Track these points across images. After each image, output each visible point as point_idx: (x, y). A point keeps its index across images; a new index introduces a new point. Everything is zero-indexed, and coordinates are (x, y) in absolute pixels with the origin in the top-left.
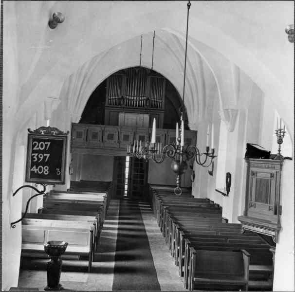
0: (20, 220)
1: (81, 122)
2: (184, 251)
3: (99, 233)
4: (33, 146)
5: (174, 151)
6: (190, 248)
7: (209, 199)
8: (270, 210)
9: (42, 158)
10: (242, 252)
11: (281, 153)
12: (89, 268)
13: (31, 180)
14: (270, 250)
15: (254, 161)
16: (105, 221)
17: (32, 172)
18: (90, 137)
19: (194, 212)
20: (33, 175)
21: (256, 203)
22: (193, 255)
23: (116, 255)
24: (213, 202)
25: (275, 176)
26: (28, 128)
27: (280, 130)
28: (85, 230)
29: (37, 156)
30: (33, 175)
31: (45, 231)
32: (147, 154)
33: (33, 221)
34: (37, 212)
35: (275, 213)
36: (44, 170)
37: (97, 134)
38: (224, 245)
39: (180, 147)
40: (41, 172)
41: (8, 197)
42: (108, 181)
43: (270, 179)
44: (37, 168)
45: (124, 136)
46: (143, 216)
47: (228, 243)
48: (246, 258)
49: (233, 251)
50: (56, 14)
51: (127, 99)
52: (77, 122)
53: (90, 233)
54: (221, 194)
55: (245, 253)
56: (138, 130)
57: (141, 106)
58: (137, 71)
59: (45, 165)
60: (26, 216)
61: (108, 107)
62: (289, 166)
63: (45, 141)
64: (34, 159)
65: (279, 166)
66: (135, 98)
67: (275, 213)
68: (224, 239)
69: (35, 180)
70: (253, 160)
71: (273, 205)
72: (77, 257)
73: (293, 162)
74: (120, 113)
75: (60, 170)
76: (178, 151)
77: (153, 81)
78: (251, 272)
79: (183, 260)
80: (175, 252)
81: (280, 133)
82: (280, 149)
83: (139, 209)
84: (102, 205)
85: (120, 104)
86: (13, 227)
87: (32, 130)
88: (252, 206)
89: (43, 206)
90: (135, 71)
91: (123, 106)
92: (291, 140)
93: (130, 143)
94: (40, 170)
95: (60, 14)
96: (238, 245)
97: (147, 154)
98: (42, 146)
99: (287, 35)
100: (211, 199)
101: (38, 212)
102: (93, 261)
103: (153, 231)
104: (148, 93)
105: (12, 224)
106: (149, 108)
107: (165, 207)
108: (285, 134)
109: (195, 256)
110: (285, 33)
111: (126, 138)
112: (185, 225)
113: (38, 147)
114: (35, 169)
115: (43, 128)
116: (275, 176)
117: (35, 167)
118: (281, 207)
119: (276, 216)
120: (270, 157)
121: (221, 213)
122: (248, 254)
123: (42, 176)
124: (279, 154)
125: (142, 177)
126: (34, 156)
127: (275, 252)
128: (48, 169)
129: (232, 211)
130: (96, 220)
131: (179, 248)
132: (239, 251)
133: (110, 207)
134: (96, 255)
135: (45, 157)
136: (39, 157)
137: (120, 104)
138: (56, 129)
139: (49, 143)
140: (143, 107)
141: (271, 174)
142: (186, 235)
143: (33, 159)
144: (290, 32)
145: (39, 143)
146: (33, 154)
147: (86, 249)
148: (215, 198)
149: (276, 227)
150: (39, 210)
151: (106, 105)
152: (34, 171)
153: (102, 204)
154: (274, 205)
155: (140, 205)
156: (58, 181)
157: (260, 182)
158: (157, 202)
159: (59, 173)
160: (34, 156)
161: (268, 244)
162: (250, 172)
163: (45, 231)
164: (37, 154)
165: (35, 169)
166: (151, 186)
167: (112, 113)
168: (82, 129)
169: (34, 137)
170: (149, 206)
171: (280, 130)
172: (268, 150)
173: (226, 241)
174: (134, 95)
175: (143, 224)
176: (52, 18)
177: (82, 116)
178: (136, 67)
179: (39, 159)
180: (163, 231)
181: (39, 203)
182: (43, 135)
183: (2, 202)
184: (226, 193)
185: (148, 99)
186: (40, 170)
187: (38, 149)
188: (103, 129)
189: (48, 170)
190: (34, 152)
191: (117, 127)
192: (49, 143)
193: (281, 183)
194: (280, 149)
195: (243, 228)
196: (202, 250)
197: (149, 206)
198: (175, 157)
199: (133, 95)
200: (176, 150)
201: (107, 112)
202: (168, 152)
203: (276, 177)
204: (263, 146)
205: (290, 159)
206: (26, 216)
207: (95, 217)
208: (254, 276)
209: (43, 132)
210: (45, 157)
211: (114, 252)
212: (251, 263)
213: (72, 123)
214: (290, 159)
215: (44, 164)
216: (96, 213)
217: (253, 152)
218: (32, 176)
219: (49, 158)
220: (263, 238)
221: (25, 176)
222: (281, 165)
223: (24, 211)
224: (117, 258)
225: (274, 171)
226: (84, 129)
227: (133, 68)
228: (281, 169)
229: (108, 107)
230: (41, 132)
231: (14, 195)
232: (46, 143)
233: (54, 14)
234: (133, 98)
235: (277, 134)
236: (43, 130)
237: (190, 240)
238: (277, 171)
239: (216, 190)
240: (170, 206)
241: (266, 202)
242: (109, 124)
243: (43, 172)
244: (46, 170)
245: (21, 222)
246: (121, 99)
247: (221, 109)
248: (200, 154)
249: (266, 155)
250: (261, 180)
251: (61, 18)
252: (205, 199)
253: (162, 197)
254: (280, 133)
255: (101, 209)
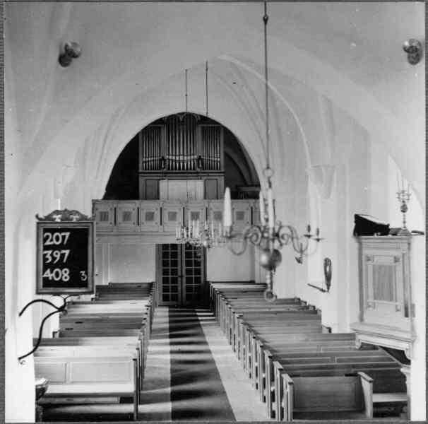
0: (30, 353)
1: (106, 197)
2: (272, 379)
3: (144, 360)
4: (45, 240)
5: (260, 235)
6: (284, 376)
7: (299, 299)
8: (398, 310)
9: (58, 257)
10: (360, 376)
11: (406, 225)
12: (135, 416)
13: (44, 291)
14: (402, 370)
15: (366, 240)
16: (150, 341)
17: (46, 280)
18: (120, 219)
19: (280, 319)
20: (47, 283)
21: (376, 301)
22: (288, 386)
23: (172, 393)
24: (306, 303)
25: (401, 260)
26: (36, 213)
27: (403, 192)
28: (126, 358)
29: (52, 255)
30: (47, 283)
31: (66, 365)
32: (208, 239)
33: (47, 349)
34: (51, 336)
35: (406, 315)
36: (62, 275)
37: (130, 213)
38: (333, 367)
39: (268, 229)
40: (59, 279)
41: (13, 316)
42: (150, 281)
43: (394, 264)
44: (52, 272)
45: (169, 213)
46: (205, 330)
47: (336, 364)
48: (367, 386)
49: (347, 375)
50: (70, 45)
51: (169, 160)
52: (100, 197)
53: (133, 362)
54: (318, 290)
55: (364, 378)
56: (190, 205)
57: (191, 169)
58: (181, 119)
59: (64, 268)
60: (41, 343)
61: (144, 173)
62: (420, 243)
63: (61, 231)
64: (47, 259)
65: (406, 245)
66: (181, 158)
67: (406, 315)
68: (329, 358)
69: (51, 290)
70: (366, 239)
71: (401, 305)
72: (116, 399)
73: (423, 239)
74: (161, 182)
75: (86, 273)
76: (266, 235)
77: (204, 131)
78: (376, 405)
79: (273, 394)
80: (258, 381)
81: (403, 196)
82: (404, 219)
83: (198, 320)
84: (145, 319)
85: (161, 168)
86: (21, 363)
87: (41, 216)
88: (369, 306)
89: (60, 326)
90: (179, 118)
91: (165, 170)
92: (421, 203)
93: (180, 223)
94: (57, 275)
95: (75, 44)
96: (354, 366)
97: (208, 239)
98: (57, 239)
99: (407, 54)
100: (301, 299)
101: (54, 336)
102: (140, 404)
103: (223, 352)
104: (200, 151)
105: (20, 358)
106: (199, 169)
107: (237, 315)
108: (411, 197)
109: (292, 389)
110: (403, 51)
111: (173, 216)
112: (259, 332)
113: (52, 240)
114: (49, 274)
115: (57, 212)
116: (401, 260)
117: (48, 271)
118: (413, 306)
119: (407, 318)
120: (390, 232)
121: (320, 318)
122: (370, 379)
123: (61, 284)
124: (405, 227)
125: (198, 272)
126: (46, 255)
127: (409, 374)
128: (68, 272)
129: (337, 313)
130: (139, 342)
131: (264, 375)
132: (355, 375)
133: (154, 320)
134: (143, 394)
135: (63, 255)
136: (55, 255)
137: (161, 168)
138: (77, 212)
139: (67, 234)
140: (194, 169)
141: (395, 258)
142: (274, 356)
143: (45, 259)
144: (411, 51)
145: (53, 235)
146: (45, 252)
147: (130, 388)
148: (311, 298)
149: (408, 336)
150: (54, 333)
151: (140, 171)
152: (48, 278)
153: (145, 316)
154: (402, 301)
155: (198, 314)
156: (83, 290)
157: (379, 269)
158: (222, 306)
159: (84, 277)
160: (46, 255)
161: (396, 361)
162: (363, 257)
163: (66, 365)
164: (50, 252)
165: (49, 274)
166: (212, 285)
167: (148, 182)
168: (109, 206)
169: (46, 227)
170: (212, 314)
171: (403, 192)
172: (386, 224)
173: (333, 360)
174: (176, 153)
175: (205, 343)
176: (64, 51)
177: (106, 189)
178: (179, 114)
179: (54, 258)
180: (237, 350)
181: (54, 325)
182: (58, 223)
183: (4, 332)
184: (325, 288)
185: (200, 158)
186: (57, 275)
187: (52, 243)
188: (138, 205)
189: (69, 275)
190: (46, 248)
191: (158, 201)
192: (67, 234)
193: (411, 271)
194: (404, 219)
195: (359, 340)
196: (301, 378)
197: (212, 314)
198: (262, 244)
199: (178, 154)
200: (263, 233)
201: (142, 180)
202: (251, 238)
203: (403, 260)
204: (375, 217)
205: (422, 234)
206: (39, 342)
207: (137, 338)
208: (382, 411)
209: (58, 218)
210: (63, 255)
211: (167, 387)
212: (376, 390)
213: (93, 200)
214: (422, 234)
215: (61, 265)
216: (138, 331)
217: (364, 227)
218: (47, 286)
219: (68, 257)
220: (389, 353)
221: (35, 286)
222: (409, 244)
223: (37, 337)
224: (175, 396)
225: (398, 253)
226: (111, 206)
227: (175, 115)
228: (409, 249)
229: (144, 173)
230: (55, 219)
231: (20, 314)
232: (63, 234)
233: (67, 46)
234: (177, 158)
235: (399, 198)
236: (57, 215)
237: (281, 363)
238: (404, 252)
239: (309, 285)
240: (243, 313)
241: (391, 299)
242: (146, 198)
243: (61, 278)
244: (65, 275)
245: (32, 354)
246: (161, 160)
247: (310, 166)
248: (299, 236)
249: (384, 230)
250: (380, 267)
251: (77, 50)
252: (293, 299)
253: (229, 300)
254: (403, 196)
255: (144, 324)
